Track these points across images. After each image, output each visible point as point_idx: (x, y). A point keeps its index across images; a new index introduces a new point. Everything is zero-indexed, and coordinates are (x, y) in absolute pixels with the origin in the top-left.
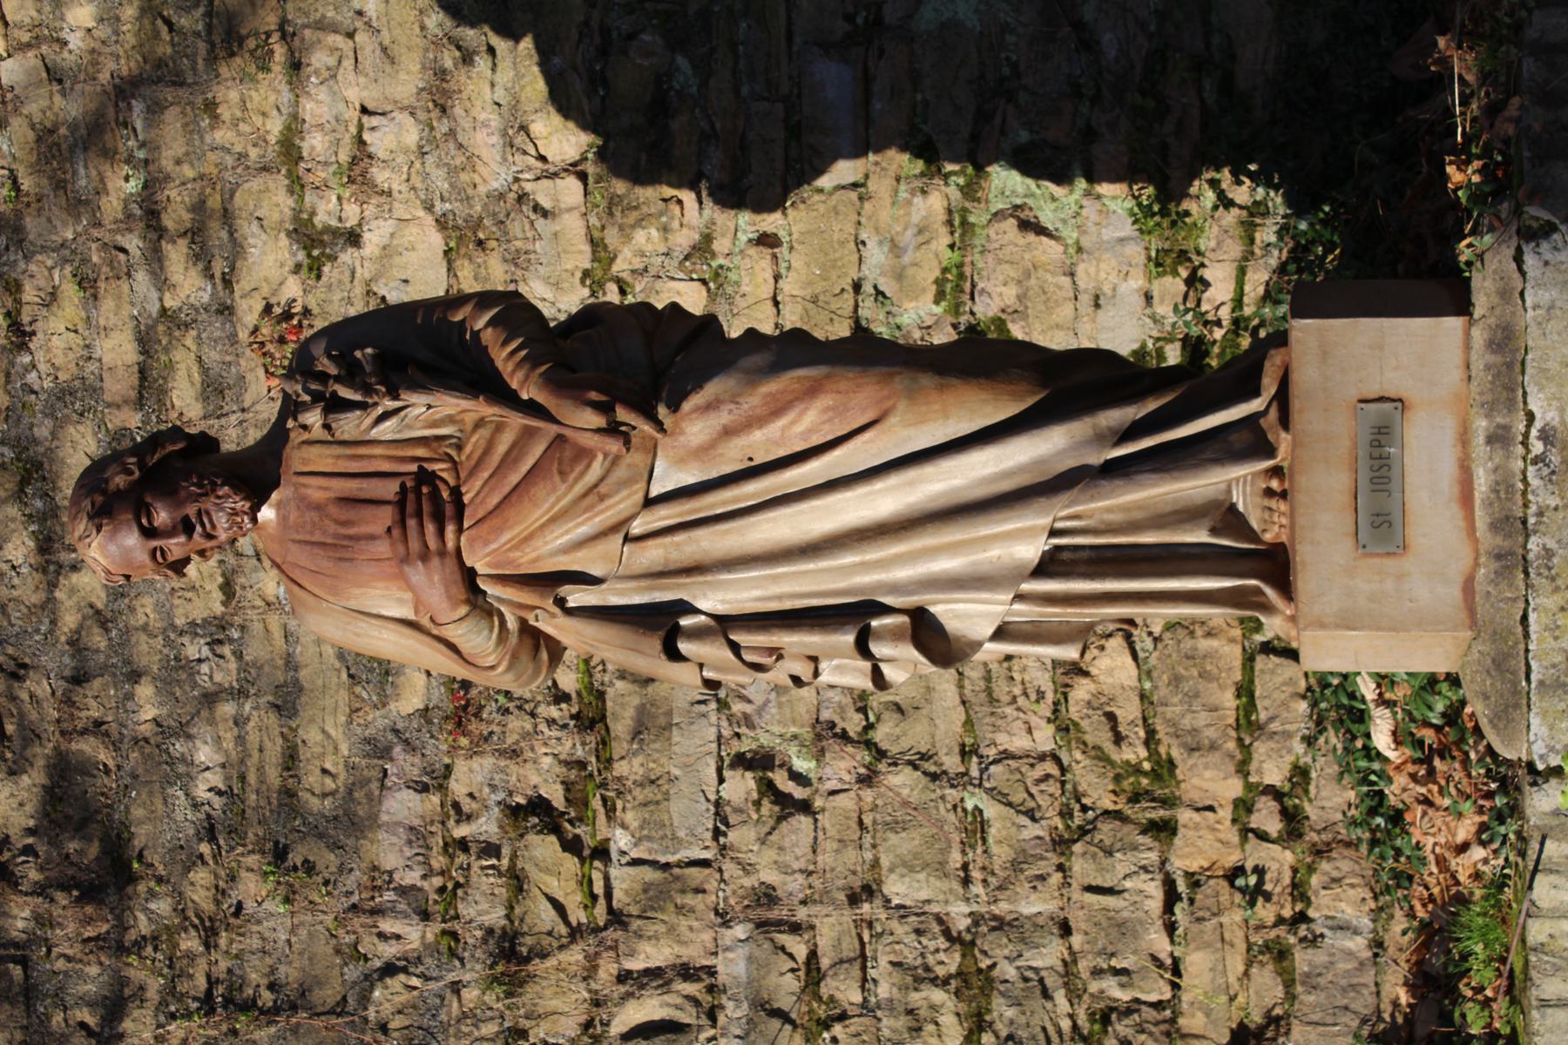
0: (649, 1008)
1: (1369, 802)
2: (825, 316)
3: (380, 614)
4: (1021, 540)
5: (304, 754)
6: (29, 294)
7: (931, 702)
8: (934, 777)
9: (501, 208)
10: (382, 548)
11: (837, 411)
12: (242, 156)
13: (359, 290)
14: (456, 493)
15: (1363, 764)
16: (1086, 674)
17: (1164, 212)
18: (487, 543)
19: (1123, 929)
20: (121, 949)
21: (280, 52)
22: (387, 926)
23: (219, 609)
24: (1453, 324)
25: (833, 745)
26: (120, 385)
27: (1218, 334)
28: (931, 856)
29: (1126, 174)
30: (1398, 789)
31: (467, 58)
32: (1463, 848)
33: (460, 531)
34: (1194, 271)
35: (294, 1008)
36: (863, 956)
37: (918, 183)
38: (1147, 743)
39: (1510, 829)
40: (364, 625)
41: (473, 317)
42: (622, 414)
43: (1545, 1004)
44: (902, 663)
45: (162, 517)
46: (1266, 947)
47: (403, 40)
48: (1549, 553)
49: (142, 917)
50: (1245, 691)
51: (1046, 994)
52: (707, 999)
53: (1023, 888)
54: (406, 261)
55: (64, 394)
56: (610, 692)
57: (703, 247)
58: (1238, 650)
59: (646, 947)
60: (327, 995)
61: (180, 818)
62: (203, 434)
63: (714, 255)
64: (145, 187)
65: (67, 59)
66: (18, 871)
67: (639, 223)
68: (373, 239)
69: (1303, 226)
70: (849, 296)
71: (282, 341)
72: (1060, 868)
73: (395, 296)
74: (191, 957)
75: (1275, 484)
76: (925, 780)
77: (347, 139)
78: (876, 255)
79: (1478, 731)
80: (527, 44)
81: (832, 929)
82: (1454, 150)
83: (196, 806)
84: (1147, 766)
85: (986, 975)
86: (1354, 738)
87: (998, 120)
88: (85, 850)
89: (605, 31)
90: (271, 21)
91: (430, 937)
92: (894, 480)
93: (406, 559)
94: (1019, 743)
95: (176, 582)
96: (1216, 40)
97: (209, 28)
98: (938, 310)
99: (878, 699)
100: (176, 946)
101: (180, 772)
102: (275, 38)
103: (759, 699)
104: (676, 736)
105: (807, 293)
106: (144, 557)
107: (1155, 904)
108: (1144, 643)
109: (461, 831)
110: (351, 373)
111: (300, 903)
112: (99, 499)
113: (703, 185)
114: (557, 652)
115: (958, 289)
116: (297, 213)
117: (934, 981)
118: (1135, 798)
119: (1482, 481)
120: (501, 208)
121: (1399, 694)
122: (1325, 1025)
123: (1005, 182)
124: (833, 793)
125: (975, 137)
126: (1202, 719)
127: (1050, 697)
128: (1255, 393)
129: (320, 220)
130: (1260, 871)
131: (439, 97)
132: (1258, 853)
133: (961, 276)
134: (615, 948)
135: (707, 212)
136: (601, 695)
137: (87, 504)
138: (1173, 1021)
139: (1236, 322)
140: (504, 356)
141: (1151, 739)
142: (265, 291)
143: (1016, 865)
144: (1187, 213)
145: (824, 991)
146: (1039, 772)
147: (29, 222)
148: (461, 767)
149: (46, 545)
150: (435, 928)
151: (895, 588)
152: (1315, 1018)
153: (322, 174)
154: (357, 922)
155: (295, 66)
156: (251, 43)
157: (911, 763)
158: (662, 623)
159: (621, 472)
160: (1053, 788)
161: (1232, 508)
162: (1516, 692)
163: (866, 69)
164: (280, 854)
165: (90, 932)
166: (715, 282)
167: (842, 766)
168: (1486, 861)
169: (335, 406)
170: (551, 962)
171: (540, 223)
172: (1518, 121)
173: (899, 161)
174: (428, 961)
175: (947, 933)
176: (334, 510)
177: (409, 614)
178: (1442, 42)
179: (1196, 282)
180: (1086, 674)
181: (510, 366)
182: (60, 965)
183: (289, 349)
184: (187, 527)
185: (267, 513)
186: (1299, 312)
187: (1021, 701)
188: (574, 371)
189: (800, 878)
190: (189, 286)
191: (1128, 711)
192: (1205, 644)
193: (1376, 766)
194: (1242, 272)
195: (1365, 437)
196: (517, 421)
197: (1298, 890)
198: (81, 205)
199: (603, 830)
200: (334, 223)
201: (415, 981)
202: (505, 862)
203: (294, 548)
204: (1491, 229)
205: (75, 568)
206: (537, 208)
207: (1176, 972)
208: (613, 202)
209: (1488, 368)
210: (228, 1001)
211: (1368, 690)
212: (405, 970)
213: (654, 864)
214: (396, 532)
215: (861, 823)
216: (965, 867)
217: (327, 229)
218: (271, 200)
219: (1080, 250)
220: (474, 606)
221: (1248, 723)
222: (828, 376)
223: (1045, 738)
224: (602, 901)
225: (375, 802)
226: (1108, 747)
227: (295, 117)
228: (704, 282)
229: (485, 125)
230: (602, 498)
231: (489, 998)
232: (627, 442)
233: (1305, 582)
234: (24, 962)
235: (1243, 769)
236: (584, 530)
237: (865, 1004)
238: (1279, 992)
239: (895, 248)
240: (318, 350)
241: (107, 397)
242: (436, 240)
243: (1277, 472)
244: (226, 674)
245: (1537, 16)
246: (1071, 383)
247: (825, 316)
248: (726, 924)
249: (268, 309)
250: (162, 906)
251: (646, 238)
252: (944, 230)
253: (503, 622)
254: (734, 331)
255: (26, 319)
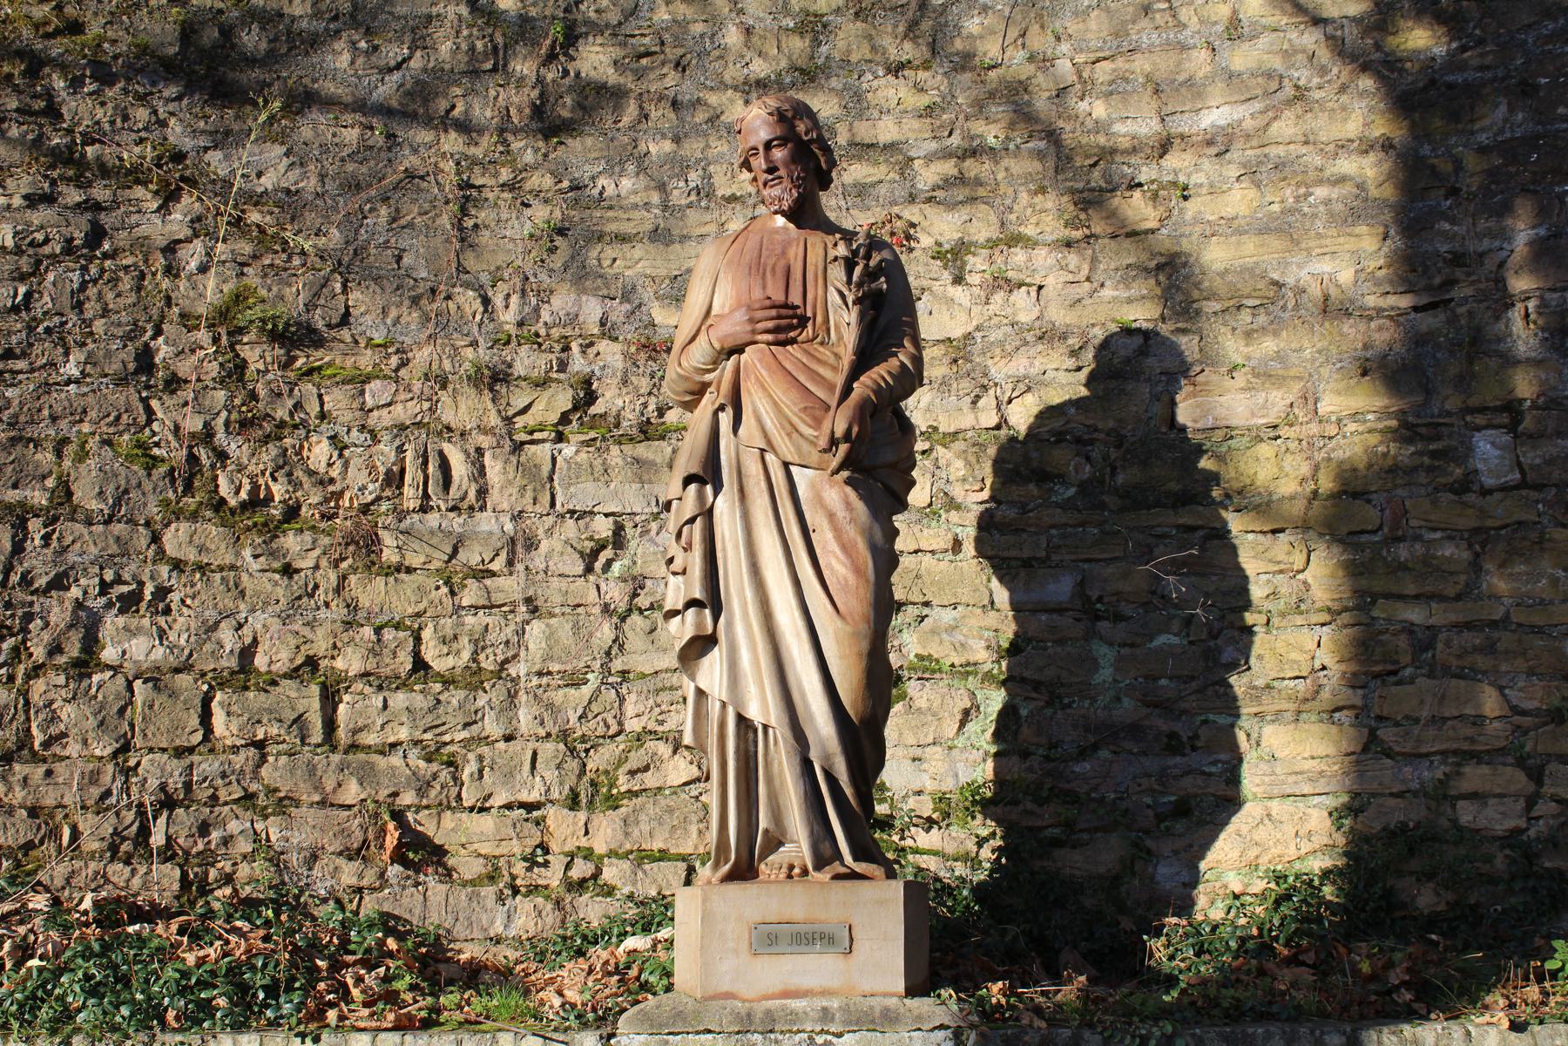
0: (460, 468)
1: (590, 935)
3: (713, 291)
4: (761, 706)
6: (922, 75)
8: (608, 653)
9: (977, 374)
10: (758, 294)
11: (845, 587)
13: (925, 283)
14: (793, 341)
15: (615, 931)
16: (675, 752)
17: (974, 803)
18: (760, 360)
19: (509, 776)
20: (501, 131)
21: (1078, 234)
22: (514, 299)
23: (719, 193)
25: (629, 587)
26: (864, 131)
27: (896, 838)
28: (557, 651)
29: (1000, 780)
30: (599, 954)
31: (1074, 353)
32: (560, 993)
33: (769, 344)
34: (936, 823)
35: (463, 240)
37: (993, 644)
38: (629, 791)
39: (573, 1022)
40: (708, 282)
42: (843, 448)
44: (682, 629)
45: (778, 154)
47: (1085, 313)
49: (522, 144)
50: (664, 856)
51: (466, 725)
52: (465, 505)
53: (536, 710)
54: (942, 313)
55: (858, 96)
57: (952, 504)
58: (690, 851)
59: (499, 466)
60: (470, 261)
61: (586, 168)
62: (831, 181)
63: (947, 511)
64: (991, 149)
65: (1072, 100)
67: (968, 463)
68: (957, 292)
69: (965, 893)
70: (921, 599)
71: (893, 234)
72: (549, 735)
73: (920, 306)
74: (496, 175)
76: (606, 647)
77: (1022, 277)
78: (948, 616)
79: (637, 1002)
80: (1084, 392)
81: (509, 587)
83: (593, 178)
84: (615, 791)
86: (632, 926)
87: (1034, 695)
88: (565, 109)
89: (1091, 442)
90: (1097, 229)
91: (507, 327)
93: (750, 309)
94: (630, 709)
95: (737, 162)
96: (1085, 836)
97: (1092, 190)
98: (912, 657)
100: (503, 165)
101: (615, 167)
102: (1087, 232)
103: (659, 539)
104: (636, 486)
105: (922, 571)
106: (751, 144)
107: (525, 797)
108: (694, 790)
109: (575, 347)
110: (870, 275)
112: (790, 114)
113: (993, 505)
114: (690, 406)
115: (925, 670)
116: (975, 244)
117: (476, 652)
118: (593, 783)
119: (797, 1004)
120: (977, 374)
121: (662, 954)
122: (437, 726)
123: (994, 700)
124: (598, 588)
125: (1023, 680)
127: (660, 729)
128: (855, 859)
129: (969, 258)
130: (546, 864)
131: (1048, 335)
132: (557, 863)
133: (934, 672)
134: (499, 446)
135: (975, 507)
136: (662, 438)
137: (787, 107)
138: (449, 807)
139: (903, 850)
140: (881, 373)
142: (924, 224)
143: (550, 706)
144: (974, 818)
145: (469, 581)
146: (611, 721)
148: (617, 347)
149: (762, 85)
150: (513, 331)
151: (730, 624)
152: (451, 899)
153: (999, 260)
154: (517, 281)
155: (1069, 244)
156: (1083, 216)
157: (617, 638)
158: (708, 474)
159: (805, 446)
160: (601, 731)
161: (781, 844)
162: (661, 1026)
163: (1067, 610)
165: (513, 111)
166: (930, 512)
167: (616, 593)
168: (551, 1007)
169: (850, 265)
170: (490, 405)
171: (968, 400)
172: (1031, 1026)
173: (1009, 630)
174: (492, 326)
175: (506, 661)
176: (782, 263)
177: (715, 310)
178: (1083, 978)
179: (930, 823)
180: (675, 752)
181: (875, 376)
182: (492, 93)
183: (887, 238)
184: (771, 170)
185: (780, 221)
187: (657, 710)
188: (872, 416)
189: (543, 566)
190: (928, 176)
191: (650, 780)
192: (694, 829)
193: (614, 940)
194: (935, 853)
195: (827, 929)
196: (839, 380)
198: (979, 106)
200: (968, 268)
201: (478, 317)
202: (555, 376)
203: (758, 238)
204: (961, 1010)
205: (747, 102)
206: (978, 397)
207: (482, 810)
209: (871, 1008)
210: (467, 198)
211: (664, 934)
212: (486, 311)
213: (553, 471)
214: (768, 303)
215: (579, 606)
216: (549, 673)
217: (964, 263)
218: (983, 228)
219: (950, 748)
220: (719, 353)
221: (642, 857)
222: (867, 581)
223: (633, 725)
224: (529, 438)
227: (1036, 244)
228: (930, 505)
229: (1031, 364)
230: (789, 435)
231: (467, 365)
232: (825, 451)
233: (734, 888)
234: (494, 70)
235: (612, 854)
236: (769, 424)
237: (461, 607)
238: (468, 877)
240: (886, 254)
241: (856, 124)
242: (957, 333)
243: (805, 872)
244: (678, 197)
245: (1098, 1038)
246: (863, 741)
248: (513, 518)
249: (913, 225)
250: (529, 157)
251: (958, 468)
252: (963, 660)
253: (709, 371)
254: (899, 521)
255: (906, 73)
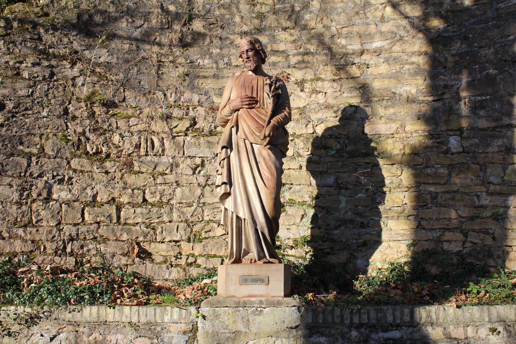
2: (286, 178)
3: (231, 93)
4: (244, 213)
5: (206, 80)
6: (292, 31)
7: (212, 197)
8: (199, 197)
9: (307, 118)
10: (244, 94)
12: (317, 70)
13: (292, 91)
14: (254, 108)
15: (201, 278)
16: (218, 226)
17: (305, 242)
19: (170, 232)
20: (170, 46)
21: (337, 78)
22: (173, 95)
23: (233, 64)
24: (281, 293)
25: (206, 178)
26: (275, 47)
27: (282, 252)
29: (312, 235)
30: (196, 284)
31: (335, 112)
32: (184, 295)
33: (247, 108)
35: (158, 77)
36: (166, 184)
39: (188, 304)
40: (229, 90)
41: (286, 112)
42: (268, 139)
43: (155, 309)
44: (221, 191)
45: (250, 53)
46: (166, 259)
48: (239, 311)
49: (176, 49)
50: (215, 256)
51: (158, 218)
52: (158, 154)
55: (274, 37)
56: (216, 137)
57: (300, 155)
58: (222, 255)
60: (160, 83)
62: (265, 61)
66: (185, 27)
67: (304, 143)
68: (302, 94)
70: (290, 183)
71: (283, 77)
72: (182, 221)
73: (291, 98)
74: (168, 58)
75: (253, 261)
77: (320, 90)
78: (298, 188)
80: (338, 123)
81: (171, 178)
82: (315, 295)
85: (162, 207)
89: (340, 138)
90: (342, 76)
92: (255, 190)
93: (241, 98)
94: (206, 213)
95: (238, 55)
96: (337, 252)
97: (341, 65)
99: (214, 187)
101: (203, 56)
103: (214, 165)
105: (291, 175)
106: (242, 50)
107: (175, 239)
108: (224, 237)
109: (191, 108)
110: (276, 89)
111: (178, 79)
112: (253, 42)
113: (311, 156)
114: (224, 126)
116: (307, 80)
117: (161, 197)
118: (195, 235)
121: (214, 284)
123: (311, 212)
125: (319, 206)
126: (210, 248)
127: (214, 219)
130: (181, 258)
131: (328, 107)
132: (184, 258)
133: (294, 204)
136: (216, 135)
137: (253, 40)
138: (153, 242)
139: (284, 255)
140: (279, 117)
141: (206, 238)
142: (292, 74)
143: (182, 213)
147: (305, 31)
148: (203, 109)
149: (246, 33)
150: (173, 103)
151: (234, 189)
153: (314, 85)
154: (174, 89)
155: (334, 81)
156: (338, 72)
158: (229, 146)
159: (257, 138)
160: (197, 220)
161: (249, 253)
164: (187, 75)
165: (173, 40)
166: (293, 157)
167: (202, 180)
169: (270, 86)
170: (166, 125)
171: (304, 125)
173: (315, 192)
175: (170, 199)
176: (251, 85)
177: (231, 98)
178: (335, 292)
179: (292, 247)
180: (218, 226)
182: (167, 35)
183: (282, 78)
184: (248, 58)
186: (285, 265)
187: (213, 214)
189: (181, 172)
190: (293, 60)
191: (211, 234)
192: (224, 248)
194: (293, 256)
197: (177, 265)
198: (309, 40)
199: (190, 135)
201: (163, 100)
203: (244, 78)
205: (241, 38)
207: (162, 242)
208: (308, 139)
210: (160, 65)
211: (215, 279)
212: (165, 98)
214: (246, 96)
216: (182, 203)
217: (304, 86)
218: (309, 76)
220: (232, 111)
221: (209, 256)
223: (206, 218)
225: (197, 93)
226: (204, 230)
227: (325, 80)
230: (252, 135)
232: (263, 140)
233: (235, 266)
234: (168, 28)
236: (246, 132)
238: (158, 262)
239: (299, 191)
240: (281, 83)
242: (301, 106)
243: (255, 261)
244: (221, 65)
246: (273, 223)
247: (286, 178)
248: (172, 158)
249: (289, 74)
250: (178, 53)
251: (301, 145)
252: (302, 201)
254: (284, 160)
255: (288, 30)
